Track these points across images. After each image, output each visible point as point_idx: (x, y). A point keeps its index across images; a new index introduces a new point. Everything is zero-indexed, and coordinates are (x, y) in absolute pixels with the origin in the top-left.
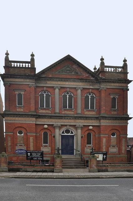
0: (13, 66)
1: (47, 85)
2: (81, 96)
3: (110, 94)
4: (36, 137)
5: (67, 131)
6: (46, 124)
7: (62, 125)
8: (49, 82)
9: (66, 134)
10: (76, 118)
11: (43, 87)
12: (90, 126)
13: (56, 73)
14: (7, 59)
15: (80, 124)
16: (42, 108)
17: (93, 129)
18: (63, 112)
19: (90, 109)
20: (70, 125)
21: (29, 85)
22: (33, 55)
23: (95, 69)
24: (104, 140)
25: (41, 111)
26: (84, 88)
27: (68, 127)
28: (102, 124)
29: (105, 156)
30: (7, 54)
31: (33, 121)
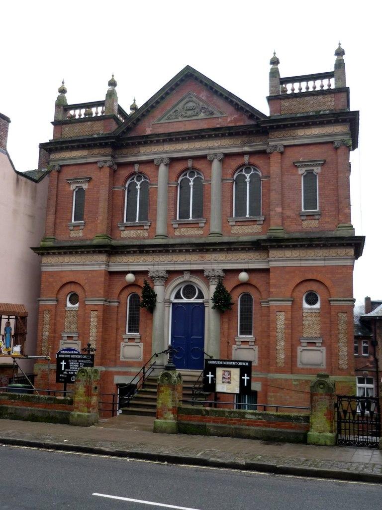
0: (289, 92)
1: (140, 158)
2: (222, 180)
3: (294, 163)
4: (106, 310)
5: (189, 290)
6: (134, 272)
7: (169, 272)
8: (143, 150)
9: (185, 300)
10: (202, 248)
11: (132, 164)
12: (241, 271)
13: (162, 121)
14: (274, 74)
15: (215, 266)
16: (241, 219)
17: (136, 280)
18: (177, 233)
19: (248, 216)
20: (192, 272)
21: (96, 163)
22: (340, 53)
23: (133, 107)
24: (281, 319)
25: (126, 234)
26: (227, 156)
27: (186, 277)
28: (273, 264)
29: (246, 378)
30: (63, 91)
31: (100, 265)
